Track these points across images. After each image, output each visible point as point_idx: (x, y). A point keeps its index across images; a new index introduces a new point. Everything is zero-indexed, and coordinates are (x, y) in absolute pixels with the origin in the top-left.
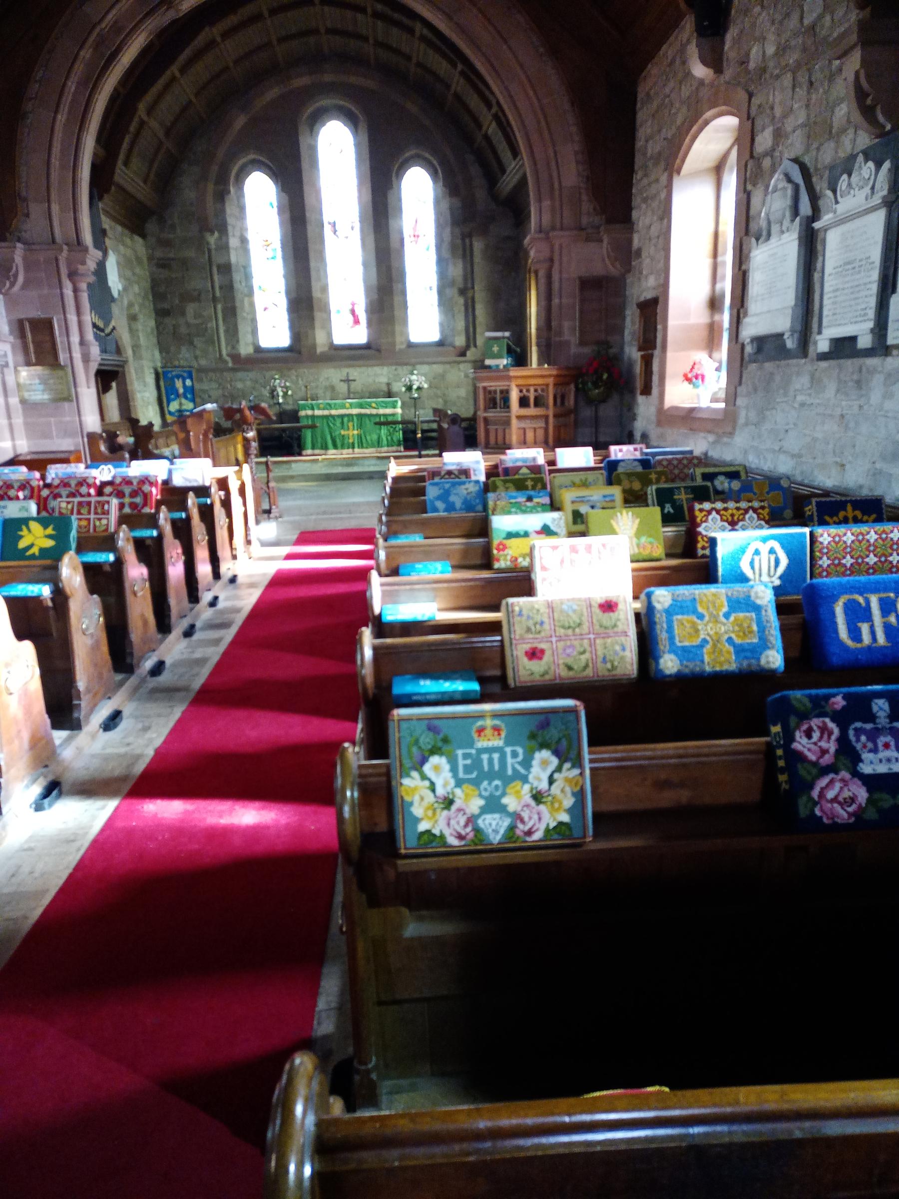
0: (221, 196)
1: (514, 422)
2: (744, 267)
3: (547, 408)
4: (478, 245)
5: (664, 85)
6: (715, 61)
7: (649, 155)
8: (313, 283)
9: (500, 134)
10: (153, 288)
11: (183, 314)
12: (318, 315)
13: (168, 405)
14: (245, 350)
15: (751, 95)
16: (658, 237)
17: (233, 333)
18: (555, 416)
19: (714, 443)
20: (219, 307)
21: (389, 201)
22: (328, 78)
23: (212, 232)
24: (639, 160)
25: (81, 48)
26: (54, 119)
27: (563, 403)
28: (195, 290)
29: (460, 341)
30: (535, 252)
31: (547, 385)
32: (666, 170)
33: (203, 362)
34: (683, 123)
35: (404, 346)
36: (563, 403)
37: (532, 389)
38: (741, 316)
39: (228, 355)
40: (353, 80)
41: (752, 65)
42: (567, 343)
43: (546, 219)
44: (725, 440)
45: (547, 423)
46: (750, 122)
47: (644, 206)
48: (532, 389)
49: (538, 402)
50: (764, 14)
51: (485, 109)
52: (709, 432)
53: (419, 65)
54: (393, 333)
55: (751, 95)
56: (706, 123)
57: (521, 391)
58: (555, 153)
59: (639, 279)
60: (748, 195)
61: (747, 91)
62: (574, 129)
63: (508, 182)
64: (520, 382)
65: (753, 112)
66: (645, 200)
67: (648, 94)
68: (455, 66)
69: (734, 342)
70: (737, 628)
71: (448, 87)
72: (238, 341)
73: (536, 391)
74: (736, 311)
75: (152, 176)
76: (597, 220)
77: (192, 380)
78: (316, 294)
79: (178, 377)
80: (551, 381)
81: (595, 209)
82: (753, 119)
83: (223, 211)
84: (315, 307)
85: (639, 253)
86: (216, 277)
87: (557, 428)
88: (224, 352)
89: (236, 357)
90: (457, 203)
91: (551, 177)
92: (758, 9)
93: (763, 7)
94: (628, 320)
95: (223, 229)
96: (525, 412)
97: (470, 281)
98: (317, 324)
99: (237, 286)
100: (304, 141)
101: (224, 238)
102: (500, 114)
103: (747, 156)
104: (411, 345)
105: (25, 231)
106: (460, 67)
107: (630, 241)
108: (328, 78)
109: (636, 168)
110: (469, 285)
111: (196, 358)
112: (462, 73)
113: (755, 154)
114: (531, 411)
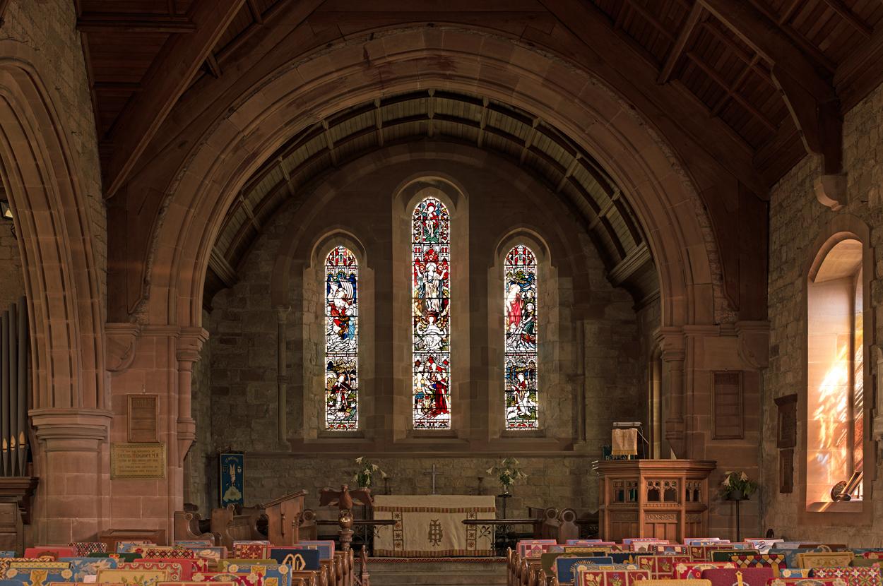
0: (299, 272)
1: (642, 515)
2: (873, 372)
3: (680, 502)
4: (591, 327)
5: (796, 201)
6: (842, 197)
7: (784, 260)
8: (395, 364)
9: (621, 218)
10: (212, 365)
11: (244, 393)
12: (397, 398)
13: (223, 497)
14: (309, 435)
15: (871, 229)
16: (795, 337)
17: (297, 416)
18: (687, 512)
19: (854, 535)
20: (284, 387)
21: (489, 278)
22: (429, 155)
23: (286, 307)
24: (773, 264)
25: (222, 152)
26: (188, 212)
27: (696, 499)
28: (259, 368)
29: (567, 432)
30: (664, 339)
31: (680, 479)
32: (800, 275)
33: (259, 447)
34: (815, 238)
35: (497, 436)
36: (696, 499)
37: (662, 483)
38: (874, 415)
39: (288, 440)
40: (456, 157)
41: (871, 204)
42: (701, 436)
43: (678, 313)
44: (864, 531)
45: (679, 519)
46: (871, 250)
47: (779, 305)
48: (662, 483)
49: (670, 495)
50: (877, 167)
51: (605, 195)
52: (849, 526)
53: (532, 148)
54: (486, 422)
55: (871, 229)
56: (836, 242)
57: (650, 484)
58: (641, 156)
59: (777, 376)
60: (874, 309)
61: (868, 225)
62: (707, 230)
63: (628, 266)
64: (650, 474)
65: (874, 243)
66: (781, 300)
67: (780, 205)
68: (574, 154)
69: (868, 440)
70: (714, 277)
71: (564, 170)
72: (301, 425)
73: (667, 484)
74: (868, 411)
75: (232, 252)
76: (732, 316)
77: (242, 468)
78: (398, 375)
79: (232, 462)
80: (683, 474)
81: (729, 305)
82: (874, 248)
83: (300, 286)
84: (395, 390)
85: (776, 350)
86: (284, 354)
87: (690, 524)
88: (285, 437)
89: (297, 443)
90: (568, 283)
91: (683, 272)
92: (872, 162)
93: (876, 161)
94: (767, 416)
95: (298, 305)
96: (654, 505)
97: (580, 367)
98: (396, 408)
99: (306, 364)
100: (397, 215)
101: (298, 314)
102: (622, 200)
103: (871, 278)
104: (505, 435)
105: (143, 313)
106: (579, 156)
107: (767, 338)
108: (429, 155)
109: (771, 269)
110: (580, 372)
111: (252, 442)
112: (581, 160)
113: (877, 276)
114: (661, 505)
